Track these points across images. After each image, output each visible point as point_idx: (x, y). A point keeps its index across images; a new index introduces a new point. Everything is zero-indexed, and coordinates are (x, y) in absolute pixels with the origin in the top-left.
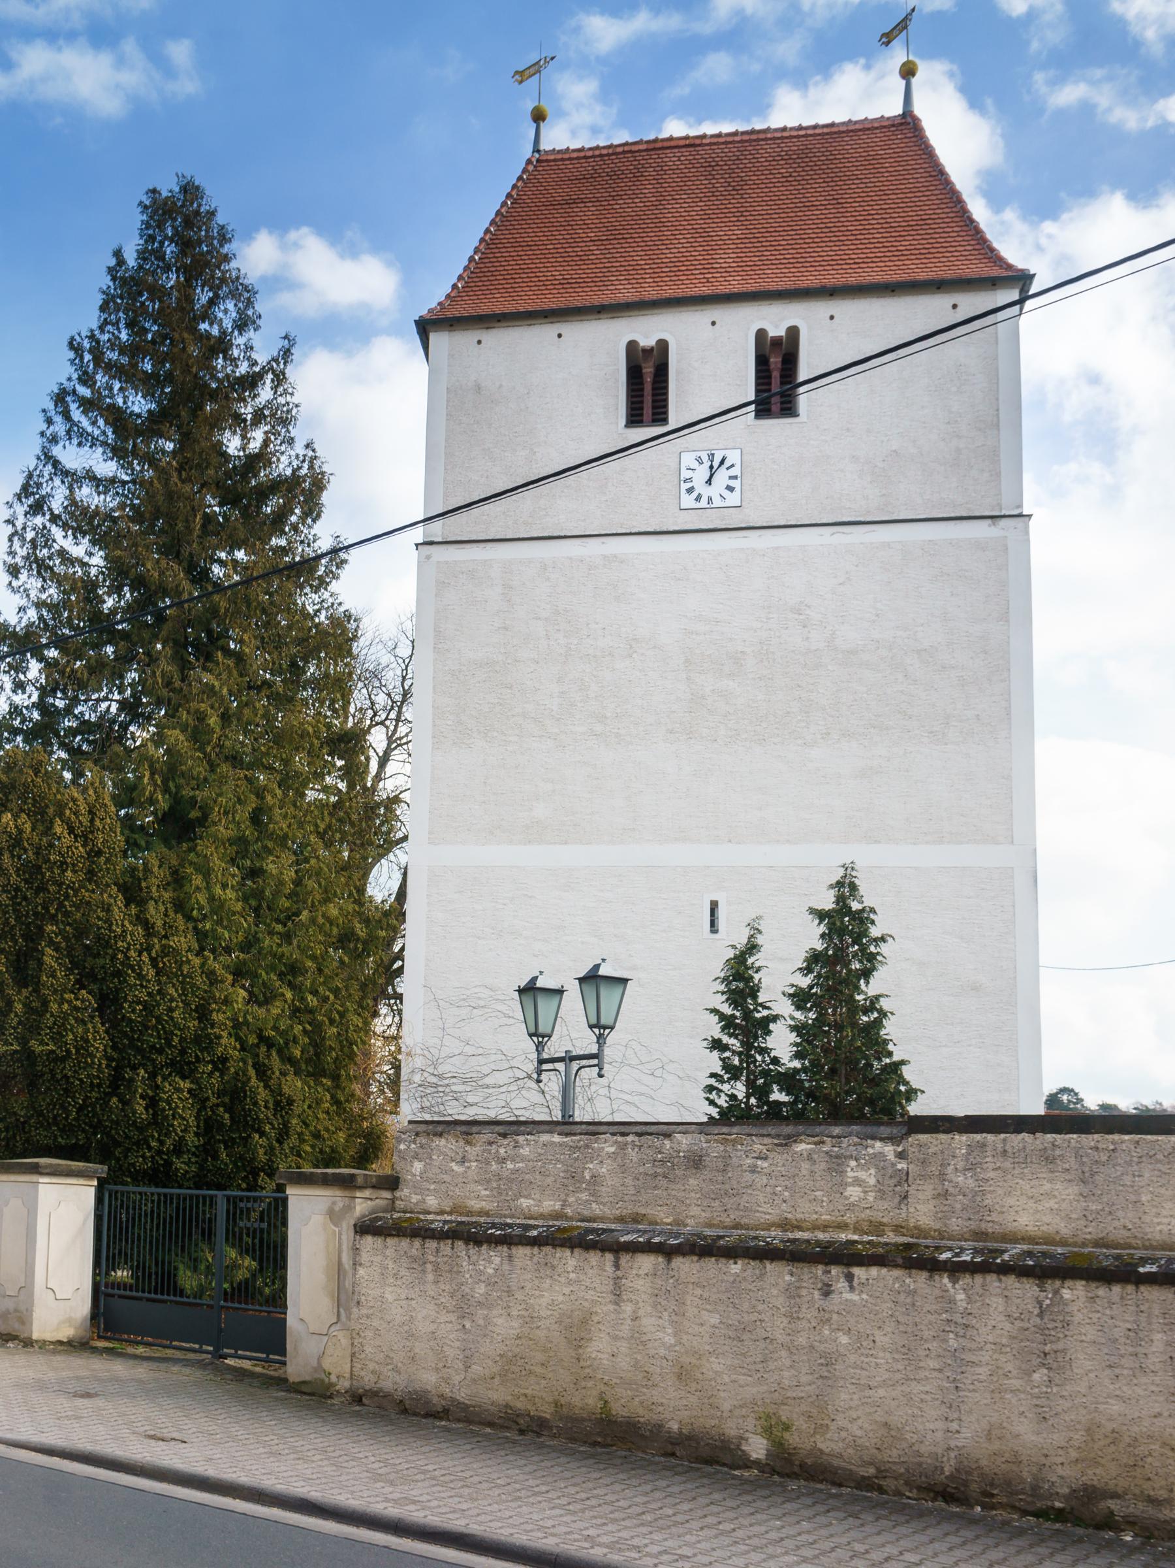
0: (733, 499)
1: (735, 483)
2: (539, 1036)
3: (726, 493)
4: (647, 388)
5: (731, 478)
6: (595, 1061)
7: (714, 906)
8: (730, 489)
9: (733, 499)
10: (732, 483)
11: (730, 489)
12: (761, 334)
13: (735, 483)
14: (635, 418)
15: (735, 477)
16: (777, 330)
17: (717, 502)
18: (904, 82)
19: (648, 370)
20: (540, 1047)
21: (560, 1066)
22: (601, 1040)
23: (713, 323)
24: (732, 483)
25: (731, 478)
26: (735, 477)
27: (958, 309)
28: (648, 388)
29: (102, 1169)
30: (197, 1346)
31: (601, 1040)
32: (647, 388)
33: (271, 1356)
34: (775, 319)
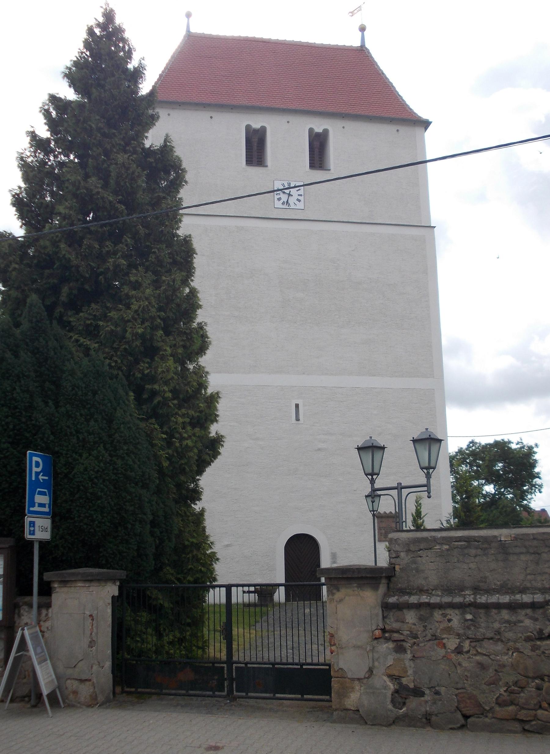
0: (301, 205)
1: (301, 198)
2: (372, 475)
3: (297, 202)
4: (256, 149)
5: (299, 195)
6: (425, 489)
7: (297, 406)
8: (299, 200)
9: (301, 205)
10: (300, 198)
11: (299, 200)
12: (311, 130)
13: (301, 198)
14: (250, 161)
15: (301, 195)
16: (319, 129)
17: (292, 206)
18: (360, 33)
19: (255, 140)
20: (372, 482)
21: (394, 493)
22: (428, 476)
23: (288, 122)
24: (300, 198)
25: (299, 195)
26: (301, 195)
27: (400, 131)
28: (255, 148)
29: (122, 574)
30: (244, 694)
31: (428, 476)
32: (256, 149)
33: (305, 696)
34: (319, 125)
